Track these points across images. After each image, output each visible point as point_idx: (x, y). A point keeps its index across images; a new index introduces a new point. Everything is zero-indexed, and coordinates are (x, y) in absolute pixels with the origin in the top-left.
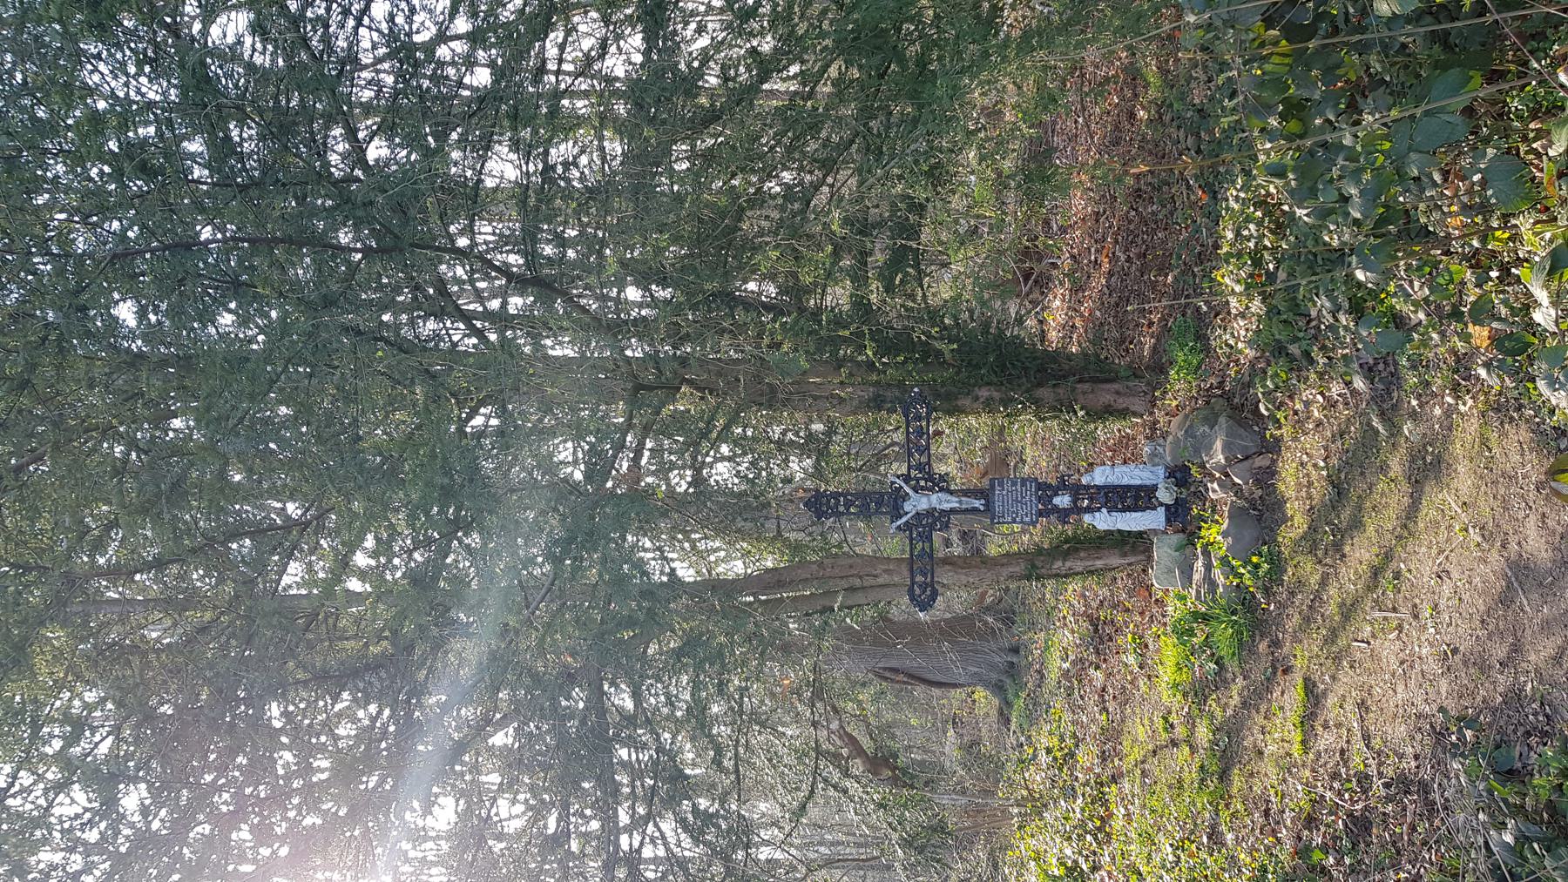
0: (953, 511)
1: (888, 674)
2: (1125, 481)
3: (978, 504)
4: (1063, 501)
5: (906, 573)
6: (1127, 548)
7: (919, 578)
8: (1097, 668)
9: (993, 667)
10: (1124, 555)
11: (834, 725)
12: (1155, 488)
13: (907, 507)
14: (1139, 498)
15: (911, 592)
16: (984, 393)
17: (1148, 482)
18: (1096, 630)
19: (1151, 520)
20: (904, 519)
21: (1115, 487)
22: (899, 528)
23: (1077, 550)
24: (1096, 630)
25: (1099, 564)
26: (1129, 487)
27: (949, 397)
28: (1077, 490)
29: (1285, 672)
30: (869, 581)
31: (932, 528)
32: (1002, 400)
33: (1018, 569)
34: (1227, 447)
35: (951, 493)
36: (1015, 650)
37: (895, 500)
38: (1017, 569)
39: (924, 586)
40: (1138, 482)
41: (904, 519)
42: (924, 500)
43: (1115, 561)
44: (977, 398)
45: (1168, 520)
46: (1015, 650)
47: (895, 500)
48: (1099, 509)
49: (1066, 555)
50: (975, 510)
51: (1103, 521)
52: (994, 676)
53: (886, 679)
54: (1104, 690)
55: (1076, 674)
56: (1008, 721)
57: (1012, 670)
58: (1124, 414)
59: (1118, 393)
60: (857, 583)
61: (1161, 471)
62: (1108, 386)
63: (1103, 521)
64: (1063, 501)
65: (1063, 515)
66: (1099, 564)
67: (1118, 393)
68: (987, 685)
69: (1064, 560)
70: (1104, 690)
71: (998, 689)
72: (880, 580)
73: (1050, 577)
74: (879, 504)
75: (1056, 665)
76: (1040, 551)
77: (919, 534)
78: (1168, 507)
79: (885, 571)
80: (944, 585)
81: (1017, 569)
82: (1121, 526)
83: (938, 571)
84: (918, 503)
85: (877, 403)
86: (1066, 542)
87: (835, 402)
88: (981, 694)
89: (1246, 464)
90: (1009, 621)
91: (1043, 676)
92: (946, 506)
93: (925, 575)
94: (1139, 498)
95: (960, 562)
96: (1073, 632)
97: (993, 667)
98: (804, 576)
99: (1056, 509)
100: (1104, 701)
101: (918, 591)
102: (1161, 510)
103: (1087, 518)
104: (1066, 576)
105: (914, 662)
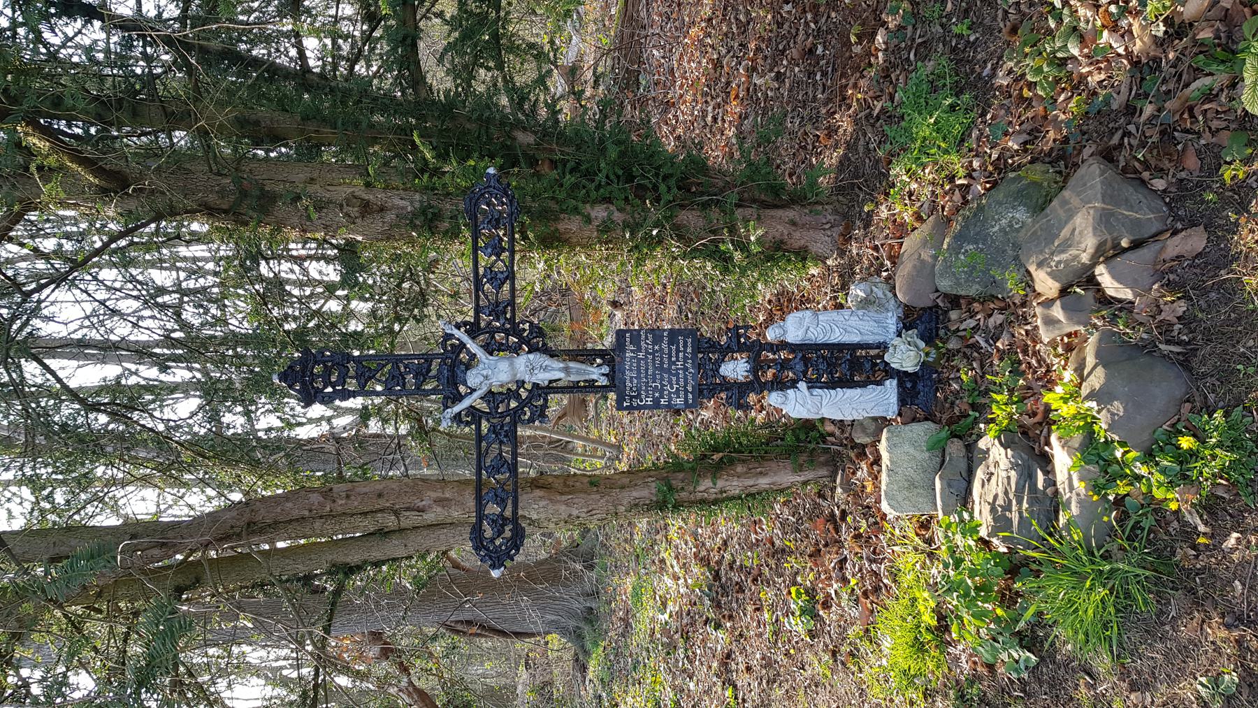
0: (552, 387)
1: (459, 627)
2: (837, 337)
3: (596, 373)
4: (736, 369)
5: (471, 503)
6: (803, 458)
7: (493, 509)
8: (718, 626)
9: (572, 614)
10: (799, 468)
11: (404, 684)
12: (883, 347)
13: (473, 378)
14: (847, 365)
15: (477, 535)
16: (599, 213)
17: (871, 339)
18: (717, 576)
19: (882, 399)
20: (466, 403)
21: (817, 347)
22: (457, 418)
23: (732, 462)
24: (717, 576)
25: (764, 482)
26: (840, 347)
27: (544, 215)
28: (755, 350)
29: (826, 605)
30: (410, 519)
31: (516, 415)
32: (626, 225)
33: (646, 492)
34: (1104, 220)
35: (552, 354)
36: (594, 594)
37: (452, 368)
38: (644, 493)
39: (499, 523)
40: (855, 338)
41: (466, 403)
42: (504, 366)
43: (787, 478)
44: (588, 220)
45: (902, 401)
46: (594, 594)
47: (452, 368)
48: (793, 384)
49: (717, 470)
50: (591, 386)
51: (798, 403)
52: (572, 623)
53: (457, 632)
54: (728, 656)
55: (684, 632)
56: (584, 669)
57: (590, 616)
58: (803, 255)
59: (793, 223)
60: (390, 521)
61: (892, 322)
62: (779, 213)
63: (798, 403)
64: (736, 369)
65: (738, 393)
66: (764, 482)
67: (793, 223)
68: (564, 631)
69: (715, 478)
70: (728, 656)
71: (577, 636)
72: (429, 517)
73: (692, 504)
74: (422, 375)
75: (650, 618)
76: (677, 466)
77: (493, 429)
78: (902, 376)
79: (438, 501)
80: (532, 522)
81: (644, 493)
82: (828, 413)
83: (523, 499)
84: (493, 372)
85: (428, 221)
86: (716, 449)
87: (354, 211)
88: (555, 640)
89: (1146, 253)
90: (589, 562)
91: (627, 625)
92: (542, 378)
93: (502, 503)
94: (847, 365)
95: (558, 484)
96: (676, 578)
97: (572, 614)
98: (296, 513)
99: (726, 385)
100: (729, 671)
101: (489, 533)
102: (891, 385)
103: (774, 399)
104: (715, 502)
105: (488, 615)
